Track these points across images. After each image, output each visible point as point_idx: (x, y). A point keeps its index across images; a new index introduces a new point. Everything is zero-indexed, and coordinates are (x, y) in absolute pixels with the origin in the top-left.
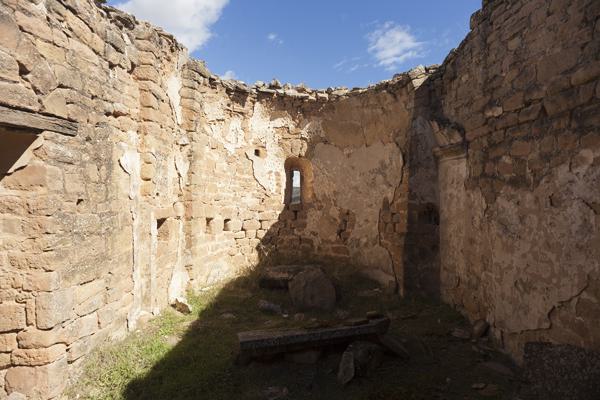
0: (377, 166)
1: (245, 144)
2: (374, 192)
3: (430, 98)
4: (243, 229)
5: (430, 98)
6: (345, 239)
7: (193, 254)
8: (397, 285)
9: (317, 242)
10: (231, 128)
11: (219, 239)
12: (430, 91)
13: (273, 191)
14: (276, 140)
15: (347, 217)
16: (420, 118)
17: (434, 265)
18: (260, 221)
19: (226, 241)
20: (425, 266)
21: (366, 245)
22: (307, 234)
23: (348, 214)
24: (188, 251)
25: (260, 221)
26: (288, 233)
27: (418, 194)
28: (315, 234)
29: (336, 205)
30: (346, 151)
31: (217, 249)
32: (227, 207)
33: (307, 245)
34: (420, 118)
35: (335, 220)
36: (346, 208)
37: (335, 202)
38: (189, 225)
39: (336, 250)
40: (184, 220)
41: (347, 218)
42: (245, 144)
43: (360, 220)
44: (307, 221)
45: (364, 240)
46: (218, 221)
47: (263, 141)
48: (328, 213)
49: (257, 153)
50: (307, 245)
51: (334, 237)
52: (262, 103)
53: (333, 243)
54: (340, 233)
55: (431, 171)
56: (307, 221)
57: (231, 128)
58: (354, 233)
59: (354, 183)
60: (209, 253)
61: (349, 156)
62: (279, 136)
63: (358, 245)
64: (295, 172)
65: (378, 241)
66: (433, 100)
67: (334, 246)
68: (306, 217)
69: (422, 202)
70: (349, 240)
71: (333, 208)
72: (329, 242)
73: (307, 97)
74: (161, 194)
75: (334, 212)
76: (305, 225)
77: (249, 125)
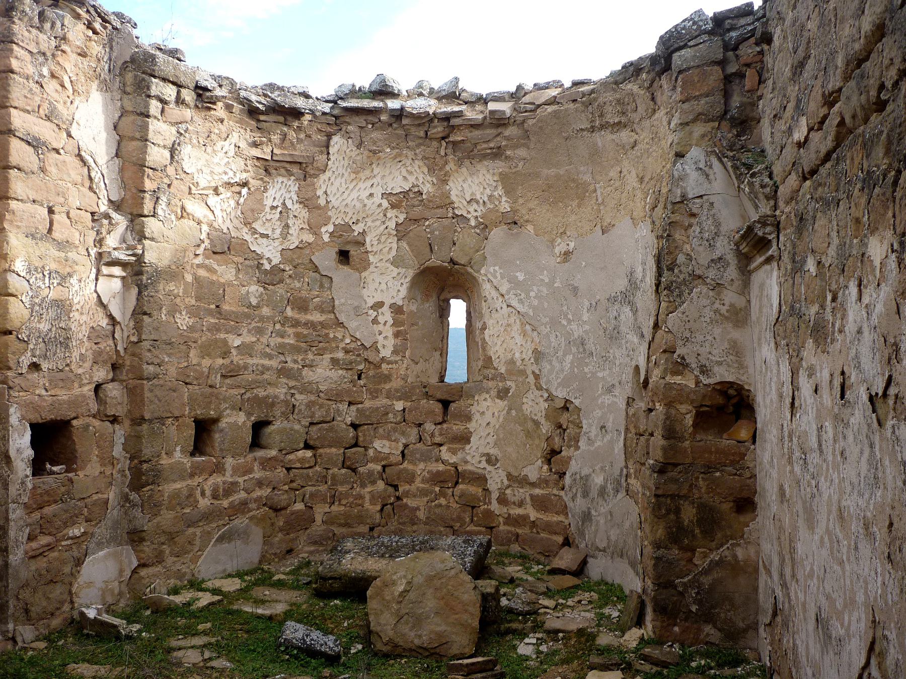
0: (622, 284)
1: (310, 238)
2: (618, 353)
3: (727, 95)
4: (307, 446)
5: (727, 95)
6: (562, 475)
7: (153, 507)
8: (642, 604)
9: (496, 479)
10: (269, 202)
11: (236, 470)
12: (728, 79)
13: (386, 353)
14: (392, 225)
15: (563, 412)
16: (695, 153)
17: (740, 553)
18: (355, 426)
19: (258, 474)
20: (715, 556)
21: (602, 492)
22: (472, 457)
23: (565, 408)
24: (134, 496)
25: (355, 426)
26: (426, 458)
27: (691, 360)
28: (491, 460)
29: (539, 388)
30: (560, 248)
31: (228, 493)
32: (262, 393)
33: (474, 490)
34: (695, 153)
35: (537, 423)
36: (561, 394)
37: (537, 377)
38: (138, 437)
39: (541, 504)
40: (127, 423)
41: (564, 419)
42: (310, 238)
43: (590, 426)
44: (472, 426)
45: (598, 480)
46: (234, 426)
47: (358, 228)
48: (520, 410)
49: (344, 256)
50: (474, 490)
51: (535, 470)
52: (348, 136)
53: (533, 485)
54: (552, 455)
55: (730, 297)
56: (472, 426)
57: (269, 202)
58: (577, 463)
59: (577, 331)
60: (204, 503)
61: (567, 254)
62: (396, 217)
63: (585, 494)
64: (452, 301)
65: (621, 484)
66: (736, 101)
67: (537, 491)
68: (468, 418)
69: (705, 380)
70: (568, 479)
71: (533, 394)
72: (523, 481)
73: (459, 114)
74: (45, 366)
75: (535, 406)
76: (465, 439)
77: (320, 192)
